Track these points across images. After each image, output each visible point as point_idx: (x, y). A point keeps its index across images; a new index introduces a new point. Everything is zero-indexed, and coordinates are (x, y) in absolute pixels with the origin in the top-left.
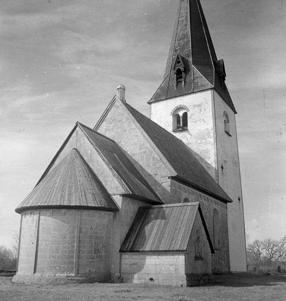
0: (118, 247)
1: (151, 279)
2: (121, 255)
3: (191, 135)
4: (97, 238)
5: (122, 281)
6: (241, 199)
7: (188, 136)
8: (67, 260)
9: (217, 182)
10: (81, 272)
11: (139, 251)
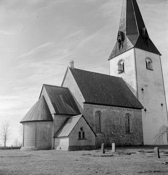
0: (53, 136)
1: (60, 148)
2: (54, 139)
3: (126, 74)
4: (44, 132)
5: (54, 149)
6: (164, 105)
7: (125, 75)
8: (32, 142)
9: (137, 98)
10: (37, 146)
11: (57, 137)
